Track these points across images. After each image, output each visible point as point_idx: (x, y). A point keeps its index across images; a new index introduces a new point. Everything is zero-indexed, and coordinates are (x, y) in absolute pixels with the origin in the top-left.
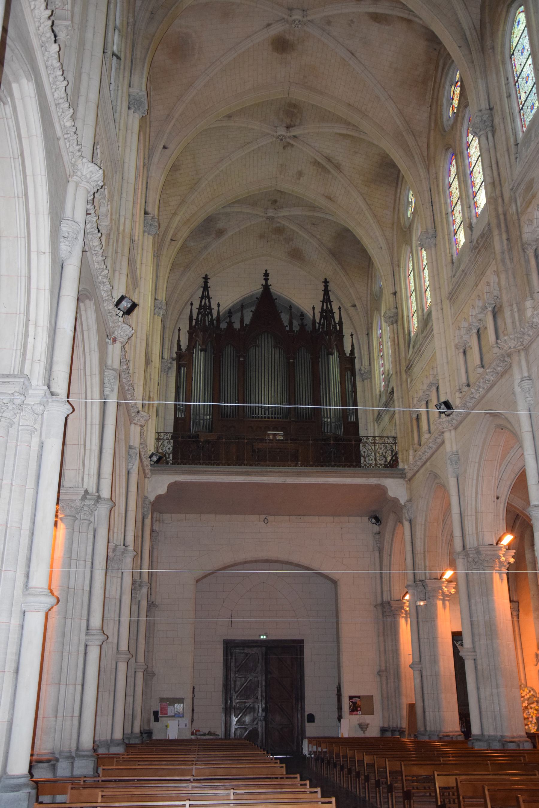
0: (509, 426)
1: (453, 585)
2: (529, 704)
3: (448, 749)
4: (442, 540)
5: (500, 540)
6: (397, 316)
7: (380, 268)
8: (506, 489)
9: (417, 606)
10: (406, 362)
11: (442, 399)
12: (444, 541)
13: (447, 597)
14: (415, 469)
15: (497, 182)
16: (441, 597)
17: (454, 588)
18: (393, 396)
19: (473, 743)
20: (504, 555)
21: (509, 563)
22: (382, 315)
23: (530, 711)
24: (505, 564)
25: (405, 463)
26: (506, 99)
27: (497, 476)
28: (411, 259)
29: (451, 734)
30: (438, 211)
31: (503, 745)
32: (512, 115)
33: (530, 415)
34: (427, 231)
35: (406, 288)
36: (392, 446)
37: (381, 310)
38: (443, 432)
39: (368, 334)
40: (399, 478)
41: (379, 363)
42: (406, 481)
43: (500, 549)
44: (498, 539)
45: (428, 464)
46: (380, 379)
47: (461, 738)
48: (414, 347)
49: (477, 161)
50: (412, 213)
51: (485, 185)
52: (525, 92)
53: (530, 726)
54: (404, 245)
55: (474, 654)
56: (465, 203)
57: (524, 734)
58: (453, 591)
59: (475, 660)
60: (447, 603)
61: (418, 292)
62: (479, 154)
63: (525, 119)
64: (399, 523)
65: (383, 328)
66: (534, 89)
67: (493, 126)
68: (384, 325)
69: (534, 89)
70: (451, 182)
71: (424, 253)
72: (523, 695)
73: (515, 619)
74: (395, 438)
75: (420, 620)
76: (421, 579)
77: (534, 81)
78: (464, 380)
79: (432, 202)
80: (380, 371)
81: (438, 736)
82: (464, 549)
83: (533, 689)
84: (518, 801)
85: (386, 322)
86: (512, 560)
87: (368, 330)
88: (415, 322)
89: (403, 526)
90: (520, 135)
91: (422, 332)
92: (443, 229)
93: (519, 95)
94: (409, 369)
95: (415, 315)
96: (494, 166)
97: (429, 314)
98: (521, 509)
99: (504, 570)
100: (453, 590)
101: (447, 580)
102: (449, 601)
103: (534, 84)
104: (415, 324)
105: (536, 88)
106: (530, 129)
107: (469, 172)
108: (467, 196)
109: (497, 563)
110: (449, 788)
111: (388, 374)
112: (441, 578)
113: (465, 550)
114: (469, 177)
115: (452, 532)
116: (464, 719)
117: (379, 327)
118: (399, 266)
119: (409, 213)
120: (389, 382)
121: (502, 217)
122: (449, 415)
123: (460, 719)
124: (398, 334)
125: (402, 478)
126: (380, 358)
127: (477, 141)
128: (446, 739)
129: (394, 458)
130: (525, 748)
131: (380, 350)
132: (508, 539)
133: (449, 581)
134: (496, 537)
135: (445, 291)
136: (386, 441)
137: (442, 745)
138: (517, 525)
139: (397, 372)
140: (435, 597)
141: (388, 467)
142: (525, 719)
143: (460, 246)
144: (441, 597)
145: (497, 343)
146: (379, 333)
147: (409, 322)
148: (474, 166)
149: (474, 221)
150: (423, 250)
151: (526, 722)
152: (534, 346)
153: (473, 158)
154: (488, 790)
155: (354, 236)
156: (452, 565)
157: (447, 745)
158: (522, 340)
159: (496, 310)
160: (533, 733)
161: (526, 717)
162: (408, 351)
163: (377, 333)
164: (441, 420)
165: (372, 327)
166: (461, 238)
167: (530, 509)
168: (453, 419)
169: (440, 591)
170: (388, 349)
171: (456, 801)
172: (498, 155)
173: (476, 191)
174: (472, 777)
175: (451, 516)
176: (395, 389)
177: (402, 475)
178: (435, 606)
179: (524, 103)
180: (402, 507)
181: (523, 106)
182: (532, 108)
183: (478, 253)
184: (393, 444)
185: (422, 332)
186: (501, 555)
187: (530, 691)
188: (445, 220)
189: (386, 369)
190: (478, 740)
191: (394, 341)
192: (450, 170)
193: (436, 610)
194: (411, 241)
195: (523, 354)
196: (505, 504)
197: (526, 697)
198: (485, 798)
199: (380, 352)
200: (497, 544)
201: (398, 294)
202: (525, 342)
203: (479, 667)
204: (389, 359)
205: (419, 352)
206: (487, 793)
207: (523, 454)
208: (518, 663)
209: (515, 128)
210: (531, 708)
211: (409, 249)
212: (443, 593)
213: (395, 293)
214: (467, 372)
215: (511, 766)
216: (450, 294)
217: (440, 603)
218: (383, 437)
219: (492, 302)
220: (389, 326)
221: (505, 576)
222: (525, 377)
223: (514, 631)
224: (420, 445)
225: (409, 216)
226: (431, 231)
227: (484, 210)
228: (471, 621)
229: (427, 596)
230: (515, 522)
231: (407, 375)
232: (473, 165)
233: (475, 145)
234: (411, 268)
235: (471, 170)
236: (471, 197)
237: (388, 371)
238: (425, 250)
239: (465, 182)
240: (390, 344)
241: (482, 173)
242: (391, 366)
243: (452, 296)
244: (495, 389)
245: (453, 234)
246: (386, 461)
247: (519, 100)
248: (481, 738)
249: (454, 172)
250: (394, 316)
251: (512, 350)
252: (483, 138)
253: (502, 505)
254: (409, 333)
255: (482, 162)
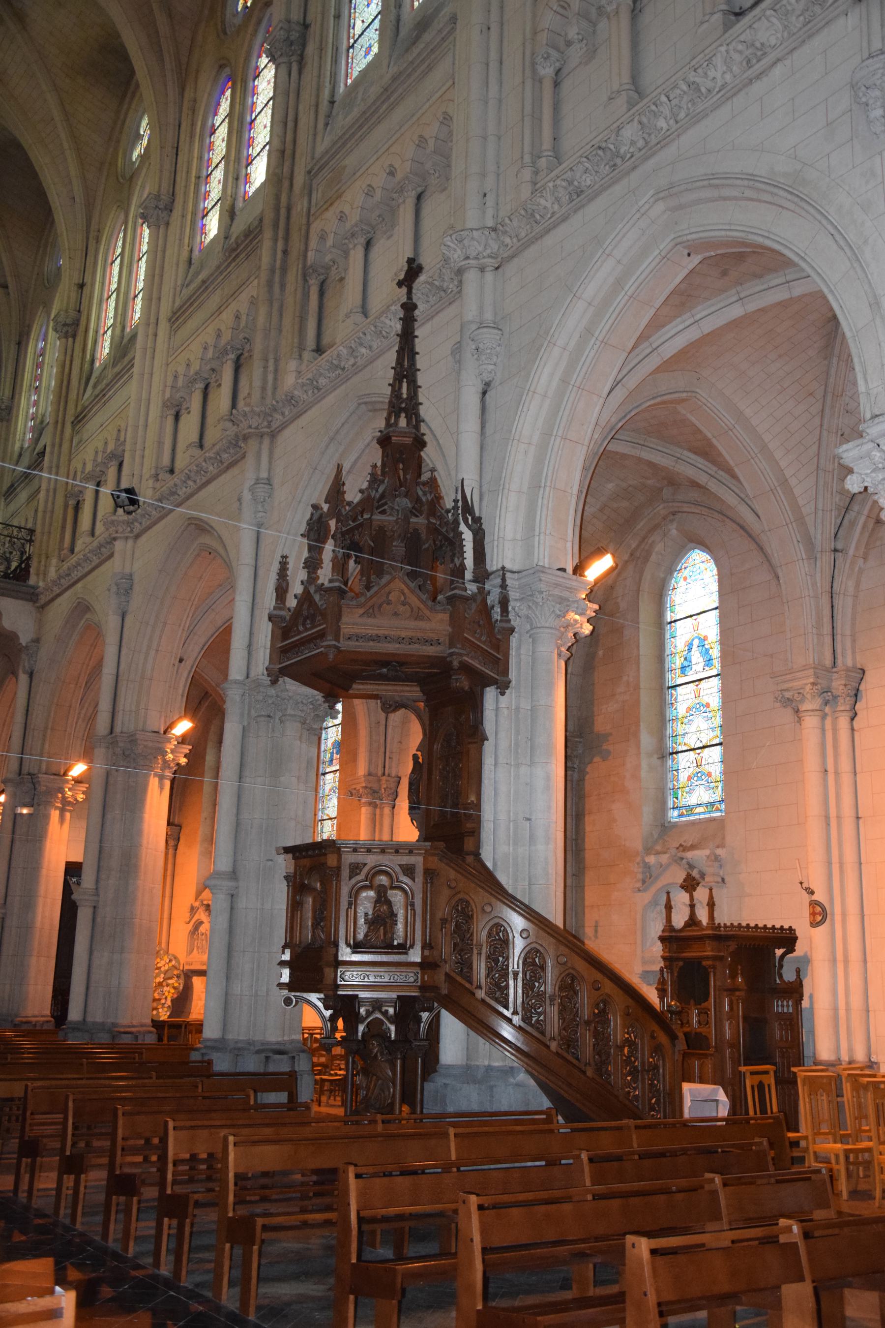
0: (222, 551)
1: (83, 787)
2: (165, 979)
3: (26, 1043)
4: (79, 713)
5: (171, 726)
6: (78, 325)
7: (65, 233)
8: (197, 649)
9: (15, 815)
10: (76, 406)
11: (124, 485)
12: (82, 715)
13: (68, 805)
14: (57, 590)
15: (288, 152)
16: (59, 805)
17: (83, 793)
18: (43, 460)
19: (66, 1034)
20: (172, 752)
21: (178, 764)
22: (52, 316)
23: (165, 989)
24: (172, 765)
25: (41, 576)
26: (332, 18)
27: (187, 626)
28: (121, 235)
29: (33, 1019)
30: (185, 169)
31: (113, 1037)
32: (336, 50)
33: (258, 533)
34: (159, 196)
35: (103, 283)
36: (23, 545)
37: (51, 308)
38: (115, 539)
39: (19, 344)
40: (27, 600)
41: (29, 399)
42: (38, 607)
43: (169, 741)
44: (168, 724)
45: (79, 585)
46: (25, 426)
47: (51, 1026)
48: (95, 387)
49: (266, 105)
50: (140, 156)
51: (269, 151)
52: (363, 21)
53: (160, 1010)
54: (115, 208)
55: (95, 898)
56: (231, 168)
57: (149, 1021)
58: (81, 797)
59: (95, 907)
60: (68, 815)
61: (122, 295)
62: (271, 94)
63: (354, 65)
64: (11, 676)
65: (49, 341)
66: (377, 21)
67: (302, 56)
68: (51, 334)
69: (377, 21)
70: (217, 125)
71: (146, 232)
72: (159, 965)
73: (171, 851)
74: (32, 532)
75: (17, 836)
76: (32, 771)
77: (380, 8)
78: (166, 461)
79: (177, 148)
80: (27, 412)
81: (12, 1021)
82: (111, 733)
83: (175, 958)
84: (115, 1115)
85: (55, 330)
86: (183, 761)
87: (21, 335)
88: (107, 344)
89: (17, 679)
90: (342, 89)
91: (114, 365)
92: (185, 202)
93: (352, 21)
94: (80, 421)
95: (109, 332)
96: (290, 125)
97: (133, 337)
98: (214, 684)
99: (169, 774)
100: (82, 796)
101: (74, 779)
102: (70, 811)
103: (379, 13)
104: (105, 349)
105: (381, 21)
106: (357, 83)
107: (248, 119)
108: (238, 160)
109: (160, 761)
110: (12, 1099)
111: (42, 422)
112: (65, 774)
113: (113, 735)
114: (248, 127)
115: (97, 705)
116: (60, 997)
117: (41, 337)
118: (98, 240)
119: (135, 155)
120: (41, 434)
121: (283, 212)
122: (129, 513)
123: (54, 997)
124: (72, 356)
125: (31, 600)
126: (33, 391)
127: (273, 72)
128: (24, 1027)
129: (23, 566)
130: (146, 1042)
131: (36, 377)
132: (183, 727)
133: (78, 781)
134: (165, 722)
135: (165, 309)
136: (15, 533)
137: (16, 1036)
138: (203, 709)
139: (57, 422)
140: (49, 804)
141: (10, 578)
142: (155, 1000)
143: (208, 240)
144: (59, 805)
145: (231, 414)
146: (40, 347)
147: (95, 342)
148: (259, 113)
149: (240, 204)
150: (145, 226)
151: (155, 1004)
152: (287, 433)
153: (260, 98)
154: (74, 1100)
155: (28, 159)
156: (87, 755)
157: (23, 1036)
158: (270, 419)
159: (242, 360)
160: (164, 1021)
161: (157, 997)
162: (85, 391)
163: (36, 346)
164: (114, 518)
165: (28, 334)
166: (213, 225)
167: (225, 685)
168: (136, 520)
169: (60, 795)
170: (50, 378)
171: (20, 1118)
172: (301, 107)
173: (254, 154)
174: (54, 1082)
175: (100, 678)
176: (48, 450)
177: (32, 596)
178: (47, 817)
179: (358, 39)
180: (20, 649)
181: (355, 42)
182: (367, 53)
183: (234, 260)
184: (27, 541)
185: (114, 365)
186: (168, 750)
187: (170, 961)
188: (192, 188)
189: (40, 412)
190: (74, 1029)
191: (63, 366)
192: (219, 104)
193: (48, 824)
194: (129, 205)
195: (266, 441)
196: (190, 671)
197: (163, 969)
198: (65, 1112)
199: (35, 381)
200: (165, 732)
201: (86, 290)
202: (275, 425)
203: (99, 920)
204: (47, 398)
205: (101, 397)
206: (71, 1104)
207: (233, 599)
208: (162, 919)
209: (335, 74)
210: (167, 985)
211: (122, 216)
212: (64, 798)
213: (81, 286)
214: (174, 450)
215: (117, 1067)
216: (174, 313)
217: (55, 815)
218: (12, 526)
219: (239, 346)
220: (59, 338)
221: (167, 784)
222: (263, 479)
223: (165, 870)
224: (72, 551)
225: (134, 159)
226: (165, 198)
227: (258, 190)
228: (101, 847)
229: (36, 801)
230: (200, 702)
231: (73, 429)
232: (258, 110)
233: (268, 78)
234: (119, 250)
235: (253, 117)
236: (244, 162)
237: (43, 416)
238: (148, 227)
239: (240, 133)
240: (55, 370)
241: (268, 129)
242: (49, 409)
243: (177, 319)
244: (211, 488)
245: (200, 215)
246: (8, 567)
247: (352, 31)
248: (82, 1026)
249: (225, 110)
250: (72, 324)
251: (253, 430)
252: (284, 69)
253: (185, 674)
254: (93, 361)
255: (273, 109)
